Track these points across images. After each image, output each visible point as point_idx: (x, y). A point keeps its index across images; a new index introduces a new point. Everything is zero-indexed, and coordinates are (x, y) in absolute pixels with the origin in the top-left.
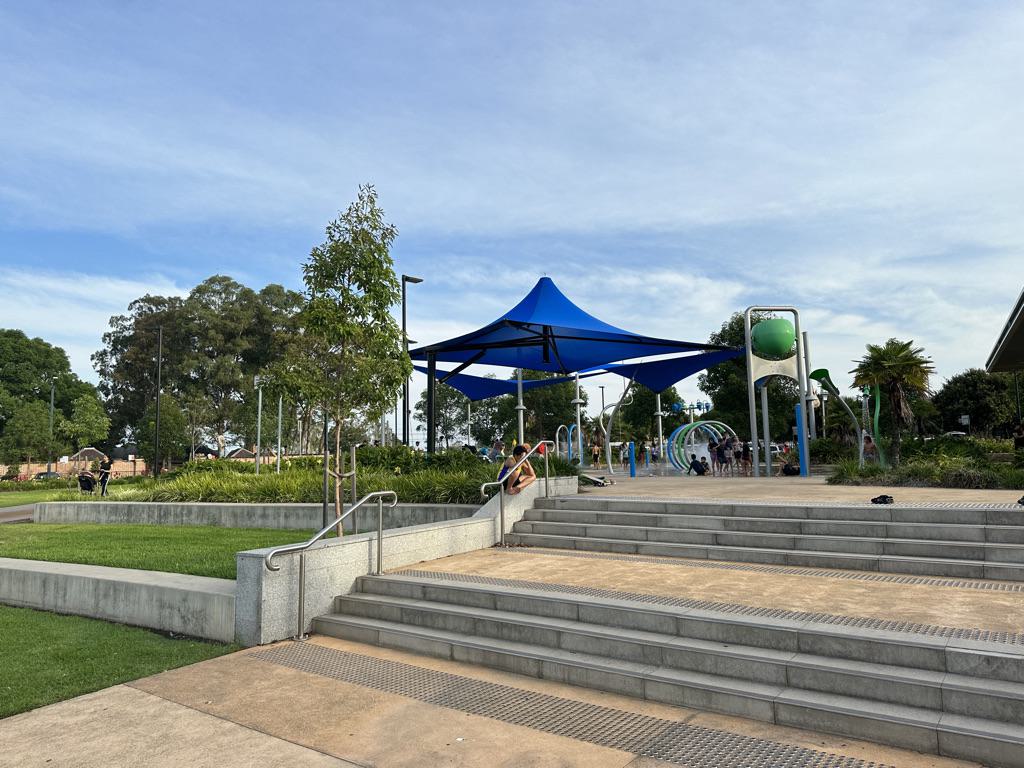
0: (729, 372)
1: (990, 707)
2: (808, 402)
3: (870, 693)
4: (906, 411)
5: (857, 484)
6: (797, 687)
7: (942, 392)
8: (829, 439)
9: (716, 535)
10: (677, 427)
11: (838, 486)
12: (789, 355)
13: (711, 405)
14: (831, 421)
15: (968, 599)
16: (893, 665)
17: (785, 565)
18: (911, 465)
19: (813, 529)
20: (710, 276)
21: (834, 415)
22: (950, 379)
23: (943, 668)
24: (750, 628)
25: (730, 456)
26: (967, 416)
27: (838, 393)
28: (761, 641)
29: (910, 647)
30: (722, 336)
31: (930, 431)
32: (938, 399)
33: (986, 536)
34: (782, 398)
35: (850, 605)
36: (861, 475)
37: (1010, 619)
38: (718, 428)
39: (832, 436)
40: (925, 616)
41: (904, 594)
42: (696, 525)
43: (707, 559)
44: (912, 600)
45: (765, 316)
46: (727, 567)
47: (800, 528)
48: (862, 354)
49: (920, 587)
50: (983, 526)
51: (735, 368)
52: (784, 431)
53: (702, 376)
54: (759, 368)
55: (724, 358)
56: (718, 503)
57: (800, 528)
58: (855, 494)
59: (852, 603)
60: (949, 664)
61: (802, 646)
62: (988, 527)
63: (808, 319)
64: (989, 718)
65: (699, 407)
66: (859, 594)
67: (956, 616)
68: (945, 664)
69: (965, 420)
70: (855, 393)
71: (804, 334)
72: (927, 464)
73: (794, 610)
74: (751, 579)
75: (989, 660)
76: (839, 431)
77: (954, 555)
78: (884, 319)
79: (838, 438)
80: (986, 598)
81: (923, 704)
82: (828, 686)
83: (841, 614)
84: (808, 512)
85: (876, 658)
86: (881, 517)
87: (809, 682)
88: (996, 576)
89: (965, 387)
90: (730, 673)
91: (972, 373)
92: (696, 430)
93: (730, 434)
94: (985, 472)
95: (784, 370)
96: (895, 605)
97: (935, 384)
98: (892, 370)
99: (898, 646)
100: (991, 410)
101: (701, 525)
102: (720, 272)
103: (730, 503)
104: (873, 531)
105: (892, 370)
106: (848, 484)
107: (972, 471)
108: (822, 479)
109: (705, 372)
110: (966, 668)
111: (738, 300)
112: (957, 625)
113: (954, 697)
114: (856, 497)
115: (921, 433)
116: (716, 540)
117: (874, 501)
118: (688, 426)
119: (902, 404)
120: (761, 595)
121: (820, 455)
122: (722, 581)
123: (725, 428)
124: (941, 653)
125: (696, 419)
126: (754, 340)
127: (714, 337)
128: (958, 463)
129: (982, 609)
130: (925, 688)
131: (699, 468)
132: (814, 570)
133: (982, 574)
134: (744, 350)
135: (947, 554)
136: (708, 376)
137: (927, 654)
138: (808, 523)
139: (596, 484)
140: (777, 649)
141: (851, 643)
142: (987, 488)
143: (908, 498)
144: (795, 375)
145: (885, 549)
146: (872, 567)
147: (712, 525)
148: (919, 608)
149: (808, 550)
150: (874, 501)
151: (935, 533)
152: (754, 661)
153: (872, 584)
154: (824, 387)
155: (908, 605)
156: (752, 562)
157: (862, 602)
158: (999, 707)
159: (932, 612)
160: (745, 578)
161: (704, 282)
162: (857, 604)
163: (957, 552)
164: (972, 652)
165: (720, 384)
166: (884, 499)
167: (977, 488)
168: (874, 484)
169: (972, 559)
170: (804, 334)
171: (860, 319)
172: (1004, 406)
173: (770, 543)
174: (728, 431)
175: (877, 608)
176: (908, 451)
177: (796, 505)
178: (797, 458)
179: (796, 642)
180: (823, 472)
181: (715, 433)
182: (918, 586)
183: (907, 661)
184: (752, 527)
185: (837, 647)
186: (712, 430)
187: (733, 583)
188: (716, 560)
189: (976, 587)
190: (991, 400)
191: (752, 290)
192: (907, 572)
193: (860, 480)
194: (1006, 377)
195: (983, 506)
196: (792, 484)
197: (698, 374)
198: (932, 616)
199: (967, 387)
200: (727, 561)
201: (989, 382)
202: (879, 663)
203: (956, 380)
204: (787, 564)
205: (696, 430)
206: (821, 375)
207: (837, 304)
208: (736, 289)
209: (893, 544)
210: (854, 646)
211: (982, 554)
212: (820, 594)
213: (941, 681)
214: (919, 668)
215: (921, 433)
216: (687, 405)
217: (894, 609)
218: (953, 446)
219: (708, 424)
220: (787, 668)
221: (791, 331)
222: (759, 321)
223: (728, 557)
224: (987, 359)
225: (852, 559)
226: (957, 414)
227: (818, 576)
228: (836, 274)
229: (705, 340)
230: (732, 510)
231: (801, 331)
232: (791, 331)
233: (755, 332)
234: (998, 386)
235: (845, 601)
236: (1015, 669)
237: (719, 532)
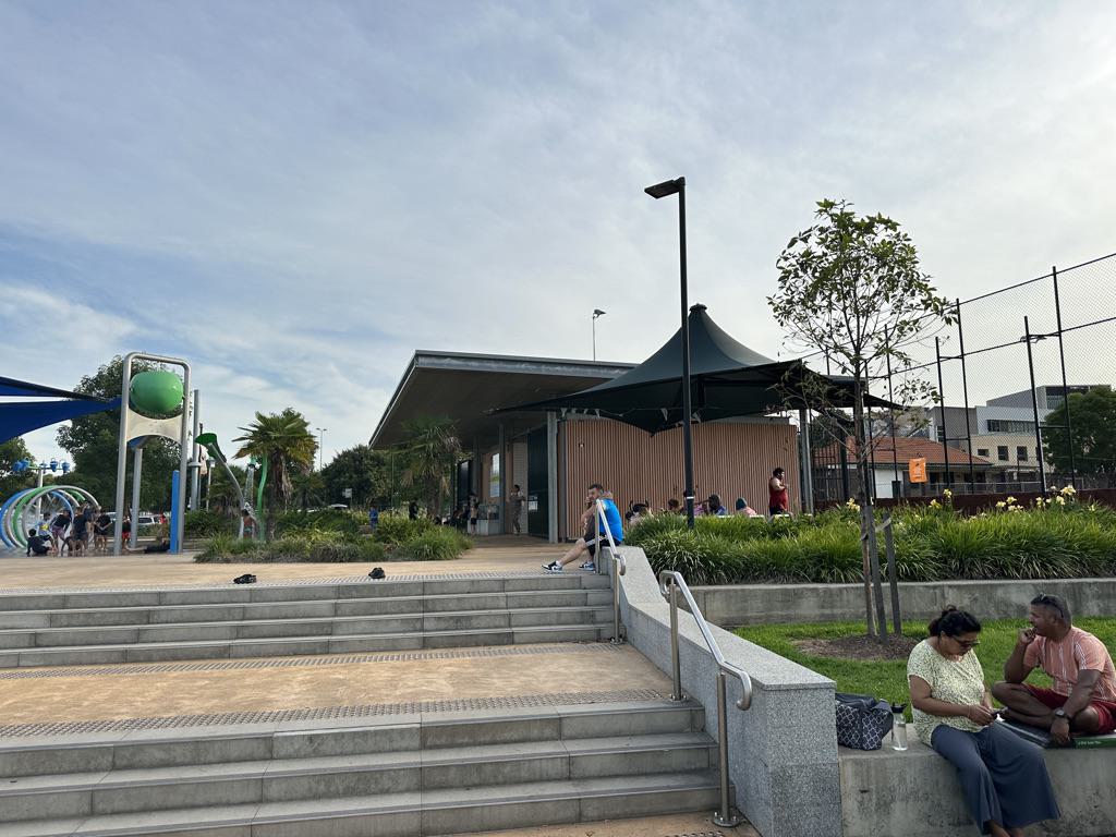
0: (102, 426)
1: (307, 786)
2: (190, 470)
3: (189, 801)
4: (286, 484)
5: (227, 561)
6: (104, 814)
7: (332, 465)
8: (211, 513)
9: (36, 634)
10: (19, 491)
11: (206, 565)
12: (173, 414)
13: (72, 466)
14: (215, 490)
15: (308, 677)
16: (219, 763)
17: (123, 663)
18: (285, 539)
19: (163, 617)
20: (92, 305)
21: (219, 484)
22: (340, 453)
23: (268, 755)
24: (50, 753)
25: (84, 530)
26: (350, 490)
27: (225, 460)
28: (66, 766)
29: (238, 739)
30: (97, 382)
31: (315, 504)
32: (325, 472)
33: (336, 611)
34: (159, 459)
35: (186, 702)
36: (232, 552)
37: (341, 692)
38: (76, 497)
39: (215, 507)
40: (264, 702)
41: (248, 681)
42: (9, 624)
43: (18, 666)
44: (256, 686)
45: (153, 365)
46: (44, 674)
47: (148, 617)
48: (250, 421)
49: (266, 670)
50: (333, 601)
51: (109, 422)
52: (159, 500)
53: (64, 428)
54: (135, 426)
55: (93, 410)
56: (47, 593)
57: (148, 617)
58: (219, 573)
59: (190, 699)
60: (276, 749)
61: (118, 762)
62: (340, 601)
63: (202, 376)
64: (304, 799)
65: (53, 467)
66: (201, 687)
67: (293, 697)
68: (271, 752)
69: (348, 493)
70: (244, 462)
71: (196, 392)
72: (300, 539)
73: (117, 719)
74: (72, 687)
75: (311, 738)
76: (224, 503)
77: (306, 632)
78: (285, 386)
79: (221, 509)
80: (325, 674)
81: (242, 799)
82: (141, 804)
83: (173, 714)
84: (160, 597)
85: (202, 759)
86: (241, 598)
87: (119, 805)
88: (339, 650)
89: (350, 463)
90: (13, 816)
91: (360, 448)
92: (44, 497)
93: (90, 502)
94: (350, 545)
95: (166, 430)
96: (235, 694)
97: (323, 459)
98: (280, 439)
99: (226, 741)
100: (372, 484)
101: (17, 623)
102: (105, 302)
103: (63, 592)
104: (229, 614)
105: (280, 439)
106: (218, 562)
107: (338, 545)
108: (189, 556)
109: (68, 423)
110: (291, 750)
111: (125, 341)
112: (290, 707)
113: (274, 785)
114: (219, 576)
115: (305, 505)
116: (35, 641)
117: (237, 581)
118: (32, 491)
119: (284, 477)
120: (79, 706)
121: (195, 528)
122: (29, 696)
123: (84, 495)
124: (268, 740)
125: (48, 481)
126: (133, 392)
127: (86, 381)
128: (325, 537)
129: (456, 680)
130: (246, 781)
131: (37, 547)
132: (156, 665)
133: (327, 649)
134: (119, 403)
135: (299, 632)
136: (73, 429)
137: (255, 743)
138: (159, 611)
139: (619, 611)
140: (87, 771)
141: (177, 748)
142: (349, 561)
143: (276, 575)
144: (177, 438)
145: (239, 632)
146: (223, 654)
147: (33, 622)
148: (256, 694)
149: (155, 642)
150: (237, 581)
151: (290, 612)
152: (48, 793)
153: (216, 673)
154: (211, 453)
155: (248, 693)
156: (81, 664)
157: (201, 696)
158: (314, 785)
159: (272, 696)
160: (64, 687)
161: (84, 312)
162: (194, 699)
163: (307, 631)
164: (297, 733)
165: (87, 439)
166: (247, 579)
167: (341, 561)
168: (245, 561)
169: (321, 635)
170: (196, 392)
171: (263, 383)
172: (382, 481)
173: (109, 638)
174: (89, 501)
175: (215, 701)
176: (284, 525)
177: (149, 590)
178: (168, 531)
179: (110, 759)
180: (190, 548)
181: (71, 501)
182: (265, 669)
183: (235, 755)
184: (88, 620)
185: (159, 755)
186: (67, 497)
187: (44, 695)
188: (29, 667)
189: (409, 658)
190: (372, 475)
191: (145, 332)
192: (258, 656)
193: (230, 556)
194: (382, 453)
195: (339, 581)
196: (156, 563)
197: (58, 425)
198: (270, 701)
199: (355, 461)
200: (46, 666)
201: (372, 458)
202: (205, 764)
203: (346, 454)
204: (126, 662)
205: (44, 497)
206: (208, 440)
207: (240, 365)
208: (125, 327)
209: (247, 626)
210: (179, 750)
211: (329, 629)
212: (154, 694)
213: (263, 771)
214: (245, 761)
215: (305, 505)
216: (37, 463)
217: (233, 699)
218: (325, 521)
219: (63, 492)
220: (92, 793)
221: (178, 387)
222: (145, 370)
223: (49, 662)
224: (369, 438)
225: (201, 648)
226: (341, 489)
227: (160, 672)
228: (242, 333)
229: (70, 386)
230: (64, 601)
231: (191, 389)
232: (178, 387)
233: (136, 384)
234: (379, 462)
235: (182, 698)
236: (333, 742)
237: (39, 630)
